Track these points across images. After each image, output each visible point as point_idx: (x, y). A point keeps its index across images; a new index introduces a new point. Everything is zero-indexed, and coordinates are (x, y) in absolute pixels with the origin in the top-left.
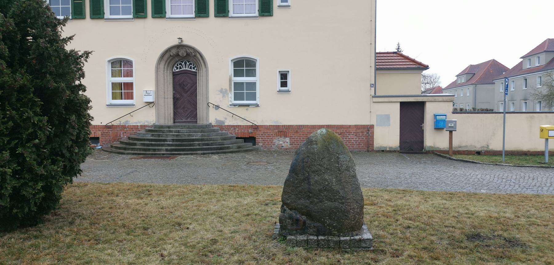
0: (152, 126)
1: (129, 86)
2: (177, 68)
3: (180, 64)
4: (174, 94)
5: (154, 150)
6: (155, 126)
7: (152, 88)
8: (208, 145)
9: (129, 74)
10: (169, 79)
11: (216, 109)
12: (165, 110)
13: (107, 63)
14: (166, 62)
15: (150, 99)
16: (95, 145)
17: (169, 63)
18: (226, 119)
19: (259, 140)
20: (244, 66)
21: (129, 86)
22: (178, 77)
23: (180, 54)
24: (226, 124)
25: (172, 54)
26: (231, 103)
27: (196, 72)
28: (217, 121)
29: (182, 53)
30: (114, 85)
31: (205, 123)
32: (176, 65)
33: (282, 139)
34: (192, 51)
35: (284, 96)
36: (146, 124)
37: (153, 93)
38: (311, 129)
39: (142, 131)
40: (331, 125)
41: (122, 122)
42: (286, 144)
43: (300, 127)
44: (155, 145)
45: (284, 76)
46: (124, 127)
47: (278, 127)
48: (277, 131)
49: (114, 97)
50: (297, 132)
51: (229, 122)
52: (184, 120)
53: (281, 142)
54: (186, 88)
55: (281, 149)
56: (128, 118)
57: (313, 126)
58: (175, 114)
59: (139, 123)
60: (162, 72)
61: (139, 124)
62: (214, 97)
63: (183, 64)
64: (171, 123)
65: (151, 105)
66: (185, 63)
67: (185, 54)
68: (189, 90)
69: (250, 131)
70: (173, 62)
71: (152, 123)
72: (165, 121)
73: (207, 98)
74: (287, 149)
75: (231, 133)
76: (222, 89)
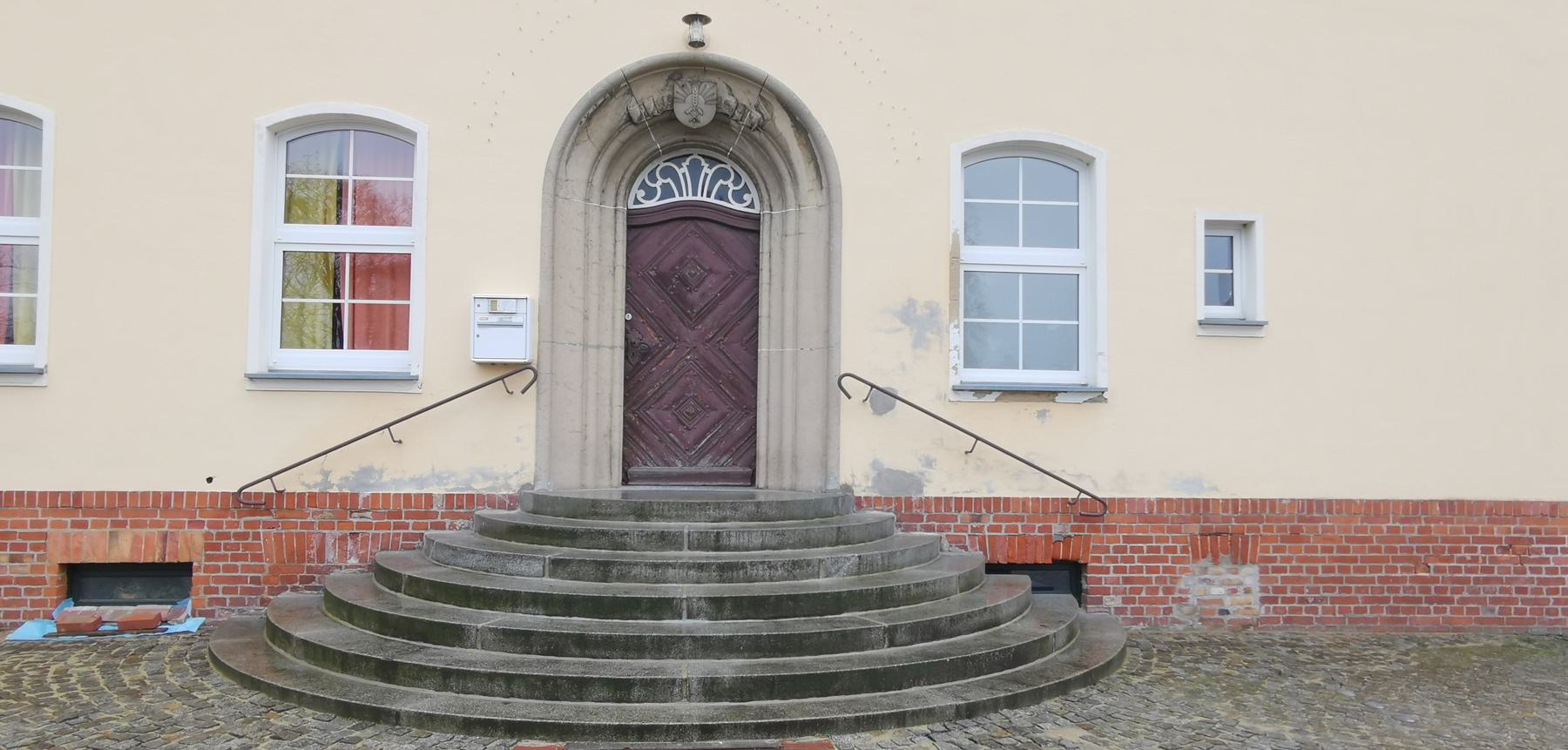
0: (513, 501)
1: (391, 273)
2: (650, 194)
3: (667, 172)
5: (621, 689)
7: (521, 283)
8: (932, 631)
9: (1065, 231)
10: (609, 247)
11: (880, 410)
13: (262, 140)
15: (514, 346)
16: (164, 609)
17: (615, 159)
18: (929, 463)
19: (1104, 574)
20: (1031, 174)
21: (391, 273)
22: (652, 241)
23: (681, 112)
24: (931, 491)
25: (636, 111)
26: (955, 381)
27: (756, 219)
28: (882, 474)
29: (694, 105)
30: (295, 262)
31: (809, 483)
32: (644, 175)
33: (1223, 571)
34: (746, 97)
35: (1230, 349)
36: (480, 487)
37: (526, 315)
38: (1367, 519)
39: (458, 533)
40: (1461, 503)
41: (339, 474)
42: (1241, 597)
43: (1312, 509)
44: (609, 646)
45: (1227, 237)
46: (346, 503)
47: (1200, 507)
48: (1195, 528)
49: (293, 332)
50: (1296, 536)
51: (948, 480)
52: (678, 467)
53: (1217, 591)
54: (694, 297)
55: (1218, 624)
56: (374, 452)
57: (1376, 504)
58: (631, 431)
59: (440, 479)
60: (578, 201)
61: (437, 490)
62: (867, 347)
63: (683, 170)
64: (592, 468)
66: (695, 170)
67: (707, 116)
68: (711, 306)
69: (1057, 529)
70: (635, 155)
71: (514, 487)
73: (829, 346)
74: (1246, 625)
75: (958, 542)
76: (912, 303)
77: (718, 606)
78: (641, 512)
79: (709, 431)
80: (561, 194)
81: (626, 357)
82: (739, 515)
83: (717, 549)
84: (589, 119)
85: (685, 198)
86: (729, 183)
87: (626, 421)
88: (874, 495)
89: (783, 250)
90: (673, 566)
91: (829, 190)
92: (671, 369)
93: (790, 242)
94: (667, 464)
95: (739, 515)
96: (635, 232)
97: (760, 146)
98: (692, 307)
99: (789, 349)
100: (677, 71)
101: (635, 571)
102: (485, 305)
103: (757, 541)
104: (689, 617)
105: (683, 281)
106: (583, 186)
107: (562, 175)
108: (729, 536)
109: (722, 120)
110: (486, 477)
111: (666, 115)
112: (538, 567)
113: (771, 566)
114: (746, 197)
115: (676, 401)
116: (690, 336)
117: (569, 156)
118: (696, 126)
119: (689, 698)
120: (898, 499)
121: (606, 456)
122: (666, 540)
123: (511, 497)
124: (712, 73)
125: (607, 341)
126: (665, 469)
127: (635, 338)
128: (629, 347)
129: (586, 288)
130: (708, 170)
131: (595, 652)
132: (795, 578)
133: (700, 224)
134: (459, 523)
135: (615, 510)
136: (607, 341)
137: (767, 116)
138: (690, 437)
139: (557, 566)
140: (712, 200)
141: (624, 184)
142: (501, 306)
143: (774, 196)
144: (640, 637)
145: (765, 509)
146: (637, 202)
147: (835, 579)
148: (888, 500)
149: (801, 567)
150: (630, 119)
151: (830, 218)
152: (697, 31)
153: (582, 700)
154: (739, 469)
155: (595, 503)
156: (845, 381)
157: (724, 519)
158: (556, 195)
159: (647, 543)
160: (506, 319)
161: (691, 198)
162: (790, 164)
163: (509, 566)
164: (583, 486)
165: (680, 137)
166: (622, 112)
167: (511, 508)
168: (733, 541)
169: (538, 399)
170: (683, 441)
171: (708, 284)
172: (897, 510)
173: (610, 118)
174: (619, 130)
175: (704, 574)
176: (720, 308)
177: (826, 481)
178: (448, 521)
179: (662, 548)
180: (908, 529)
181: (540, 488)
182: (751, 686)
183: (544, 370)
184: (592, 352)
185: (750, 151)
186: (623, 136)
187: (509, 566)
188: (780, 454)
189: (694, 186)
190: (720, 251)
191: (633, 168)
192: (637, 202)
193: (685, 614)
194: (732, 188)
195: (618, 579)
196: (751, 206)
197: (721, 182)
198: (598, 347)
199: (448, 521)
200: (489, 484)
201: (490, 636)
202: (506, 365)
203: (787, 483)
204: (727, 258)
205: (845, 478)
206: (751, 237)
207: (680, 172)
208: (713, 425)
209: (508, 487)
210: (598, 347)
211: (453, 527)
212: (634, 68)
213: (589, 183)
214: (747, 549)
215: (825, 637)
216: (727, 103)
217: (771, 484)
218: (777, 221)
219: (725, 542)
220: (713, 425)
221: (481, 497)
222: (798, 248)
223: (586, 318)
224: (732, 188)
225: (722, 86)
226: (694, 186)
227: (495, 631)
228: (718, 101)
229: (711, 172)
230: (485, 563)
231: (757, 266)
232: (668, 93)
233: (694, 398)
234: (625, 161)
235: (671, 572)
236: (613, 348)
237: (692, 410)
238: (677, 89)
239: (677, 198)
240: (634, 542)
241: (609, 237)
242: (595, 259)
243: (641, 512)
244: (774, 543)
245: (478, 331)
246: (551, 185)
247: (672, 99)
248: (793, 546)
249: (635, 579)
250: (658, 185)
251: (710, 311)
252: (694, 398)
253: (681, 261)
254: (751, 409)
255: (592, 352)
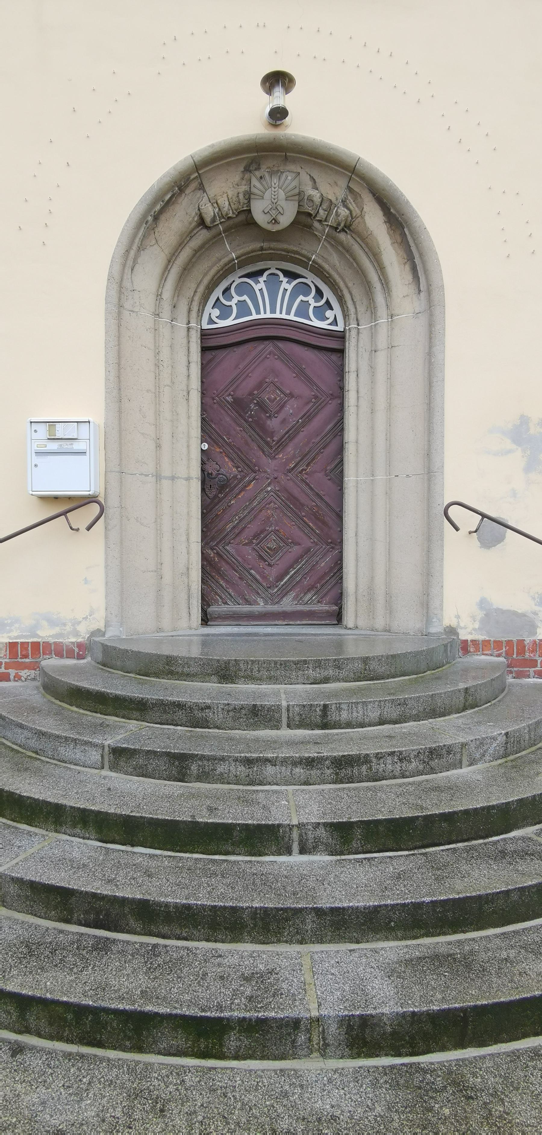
0: (81, 650)
3: (242, 289)
4: (206, 456)
6: (111, 657)
7: (84, 402)
10: (182, 369)
11: (489, 542)
12: (159, 550)
14: (170, 261)
15: (77, 477)
17: (186, 270)
22: (229, 362)
23: (259, 212)
25: (209, 212)
27: (341, 337)
28: (490, 614)
29: (274, 202)
32: (218, 292)
34: (329, 189)
36: (46, 634)
37: (90, 440)
52: (261, 606)
58: (210, 568)
64: (166, 612)
65: (82, 517)
66: (273, 286)
68: (291, 435)
71: (82, 633)
72: (524, 854)
73: (430, 472)
77: (346, 836)
78: (226, 673)
79: (291, 566)
80: (128, 305)
81: (203, 490)
82: (343, 674)
83: (325, 726)
84: (156, 218)
85: (262, 316)
86: (310, 299)
87: (204, 557)
88: (480, 637)
89: (372, 368)
90: (272, 762)
91: (429, 292)
92: (251, 501)
93: (381, 358)
94: (248, 602)
95: (343, 674)
96: (209, 355)
97: (345, 251)
98: (272, 434)
99: (380, 477)
100: (254, 157)
101: (221, 768)
102: (43, 431)
103: (374, 715)
104: (303, 851)
105: (262, 406)
106: (152, 298)
107: (127, 284)
108: (339, 709)
109: (304, 222)
110: (52, 623)
111: (242, 217)
112: (95, 756)
113: (402, 758)
114: (329, 314)
115: (256, 536)
116: (270, 465)
117: (135, 261)
118: (275, 228)
119: (324, 1051)
120: (509, 643)
121: (184, 596)
122: (259, 715)
123: (80, 645)
124: (294, 161)
125: (182, 471)
126: (246, 608)
127: (212, 468)
128: (206, 478)
129: (158, 414)
130: (287, 285)
131: (165, 930)
132: (432, 771)
133: (281, 344)
134: (24, 673)
135: (193, 670)
136: (182, 471)
137: (356, 211)
138: (273, 573)
139: (120, 757)
140: (292, 317)
141: (197, 298)
142: (60, 431)
143: (361, 309)
144: (234, 910)
145: (373, 665)
146: (211, 321)
147: (480, 766)
148: (498, 644)
149: (440, 756)
150: (202, 222)
151: (431, 325)
152: (280, 98)
153: (140, 1050)
154: (324, 607)
155: (170, 660)
156: (452, 511)
157: (326, 680)
158: (120, 306)
159: (235, 719)
160: (66, 446)
161: (269, 315)
162: (381, 269)
163: (62, 750)
164: (160, 630)
165: (257, 245)
166: (193, 212)
167: (80, 657)
168: (344, 715)
169: (106, 537)
170: (264, 577)
171: (288, 409)
172: (508, 654)
173: (179, 219)
174: (190, 235)
175: (314, 772)
176: (301, 435)
177: (428, 621)
178: (12, 672)
179: (255, 726)
180: (519, 675)
181: (114, 634)
182: (428, 1027)
183: (113, 503)
184: (166, 484)
185: (335, 258)
186: (195, 243)
187: (62, 750)
188: (371, 589)
189: (275, 301)
190: (301, 373)
191: (206, 281)
192: (211, 321)
193: (295, 847)
194: (313, 304)
195: (199, 779)
196: (335, 322)
197: (301, 298)
198: (173, 478)
199: (12, 672)
200: (56, 630)
201: (13, 889)
202: (70, 498)
203: (380, 623)
204: (309, 380)
205: (448, 619)
206: (334, 357)
207: (257, 288)
208: (296, 561)
209: (77, 634)
210: (173, 478)
211: (18, 678)
212: (206, 153)
213: (159, 296)
214: (362, 725)
215: (515, 897)
216: (310, 199)
217: (360, 623)
218: (365, 337)
219: (333, 716)
220: (296, 561)
221: (47, 644)
222: (390, 363)
223: (158, 446)
224: (313, 304)
225: (305, 178)
226: (275, 301)
227: (19, 881)
228: (300, 196)
229: (290, 287)
230: (33, 743)
231: (342, 388)
232: (243, 188)
233: (276, 532)
234: (197, 273)
235: (270, 770)
236: (188, 479)
237: (273, 545)
238: (255, 182)
239: (254, 316)
240: (218, 717)
241: (181, 358)
242: (168, 382)
243: (226, 673)
244: (394, 716)
245: (36, 460)
246: (114, 293)
247: (249, 196)
248: (417, 718)
249: (222, 779)
250: (233, 303)
251: (291, 439)
252: (276, 532)
253: (260, 386)
254: (337, 543)
255: (166, 484)
